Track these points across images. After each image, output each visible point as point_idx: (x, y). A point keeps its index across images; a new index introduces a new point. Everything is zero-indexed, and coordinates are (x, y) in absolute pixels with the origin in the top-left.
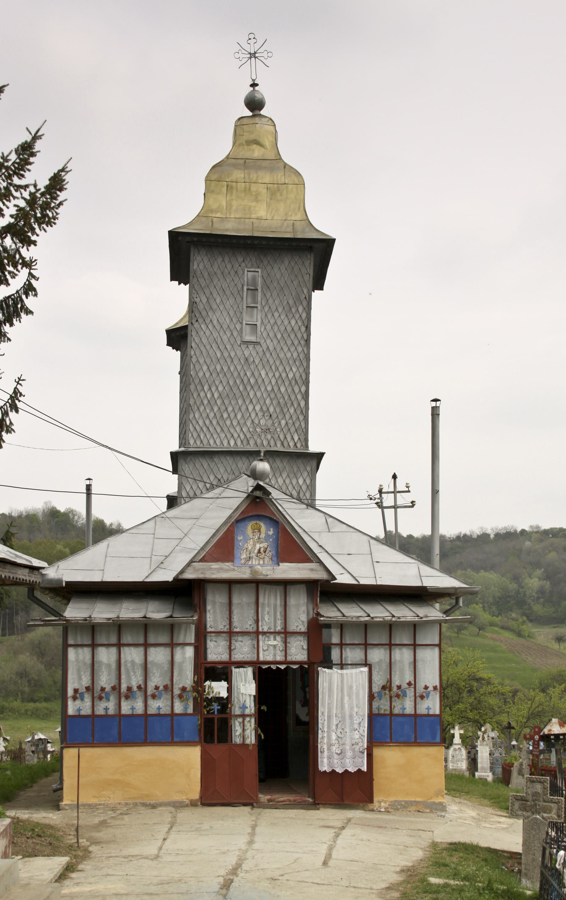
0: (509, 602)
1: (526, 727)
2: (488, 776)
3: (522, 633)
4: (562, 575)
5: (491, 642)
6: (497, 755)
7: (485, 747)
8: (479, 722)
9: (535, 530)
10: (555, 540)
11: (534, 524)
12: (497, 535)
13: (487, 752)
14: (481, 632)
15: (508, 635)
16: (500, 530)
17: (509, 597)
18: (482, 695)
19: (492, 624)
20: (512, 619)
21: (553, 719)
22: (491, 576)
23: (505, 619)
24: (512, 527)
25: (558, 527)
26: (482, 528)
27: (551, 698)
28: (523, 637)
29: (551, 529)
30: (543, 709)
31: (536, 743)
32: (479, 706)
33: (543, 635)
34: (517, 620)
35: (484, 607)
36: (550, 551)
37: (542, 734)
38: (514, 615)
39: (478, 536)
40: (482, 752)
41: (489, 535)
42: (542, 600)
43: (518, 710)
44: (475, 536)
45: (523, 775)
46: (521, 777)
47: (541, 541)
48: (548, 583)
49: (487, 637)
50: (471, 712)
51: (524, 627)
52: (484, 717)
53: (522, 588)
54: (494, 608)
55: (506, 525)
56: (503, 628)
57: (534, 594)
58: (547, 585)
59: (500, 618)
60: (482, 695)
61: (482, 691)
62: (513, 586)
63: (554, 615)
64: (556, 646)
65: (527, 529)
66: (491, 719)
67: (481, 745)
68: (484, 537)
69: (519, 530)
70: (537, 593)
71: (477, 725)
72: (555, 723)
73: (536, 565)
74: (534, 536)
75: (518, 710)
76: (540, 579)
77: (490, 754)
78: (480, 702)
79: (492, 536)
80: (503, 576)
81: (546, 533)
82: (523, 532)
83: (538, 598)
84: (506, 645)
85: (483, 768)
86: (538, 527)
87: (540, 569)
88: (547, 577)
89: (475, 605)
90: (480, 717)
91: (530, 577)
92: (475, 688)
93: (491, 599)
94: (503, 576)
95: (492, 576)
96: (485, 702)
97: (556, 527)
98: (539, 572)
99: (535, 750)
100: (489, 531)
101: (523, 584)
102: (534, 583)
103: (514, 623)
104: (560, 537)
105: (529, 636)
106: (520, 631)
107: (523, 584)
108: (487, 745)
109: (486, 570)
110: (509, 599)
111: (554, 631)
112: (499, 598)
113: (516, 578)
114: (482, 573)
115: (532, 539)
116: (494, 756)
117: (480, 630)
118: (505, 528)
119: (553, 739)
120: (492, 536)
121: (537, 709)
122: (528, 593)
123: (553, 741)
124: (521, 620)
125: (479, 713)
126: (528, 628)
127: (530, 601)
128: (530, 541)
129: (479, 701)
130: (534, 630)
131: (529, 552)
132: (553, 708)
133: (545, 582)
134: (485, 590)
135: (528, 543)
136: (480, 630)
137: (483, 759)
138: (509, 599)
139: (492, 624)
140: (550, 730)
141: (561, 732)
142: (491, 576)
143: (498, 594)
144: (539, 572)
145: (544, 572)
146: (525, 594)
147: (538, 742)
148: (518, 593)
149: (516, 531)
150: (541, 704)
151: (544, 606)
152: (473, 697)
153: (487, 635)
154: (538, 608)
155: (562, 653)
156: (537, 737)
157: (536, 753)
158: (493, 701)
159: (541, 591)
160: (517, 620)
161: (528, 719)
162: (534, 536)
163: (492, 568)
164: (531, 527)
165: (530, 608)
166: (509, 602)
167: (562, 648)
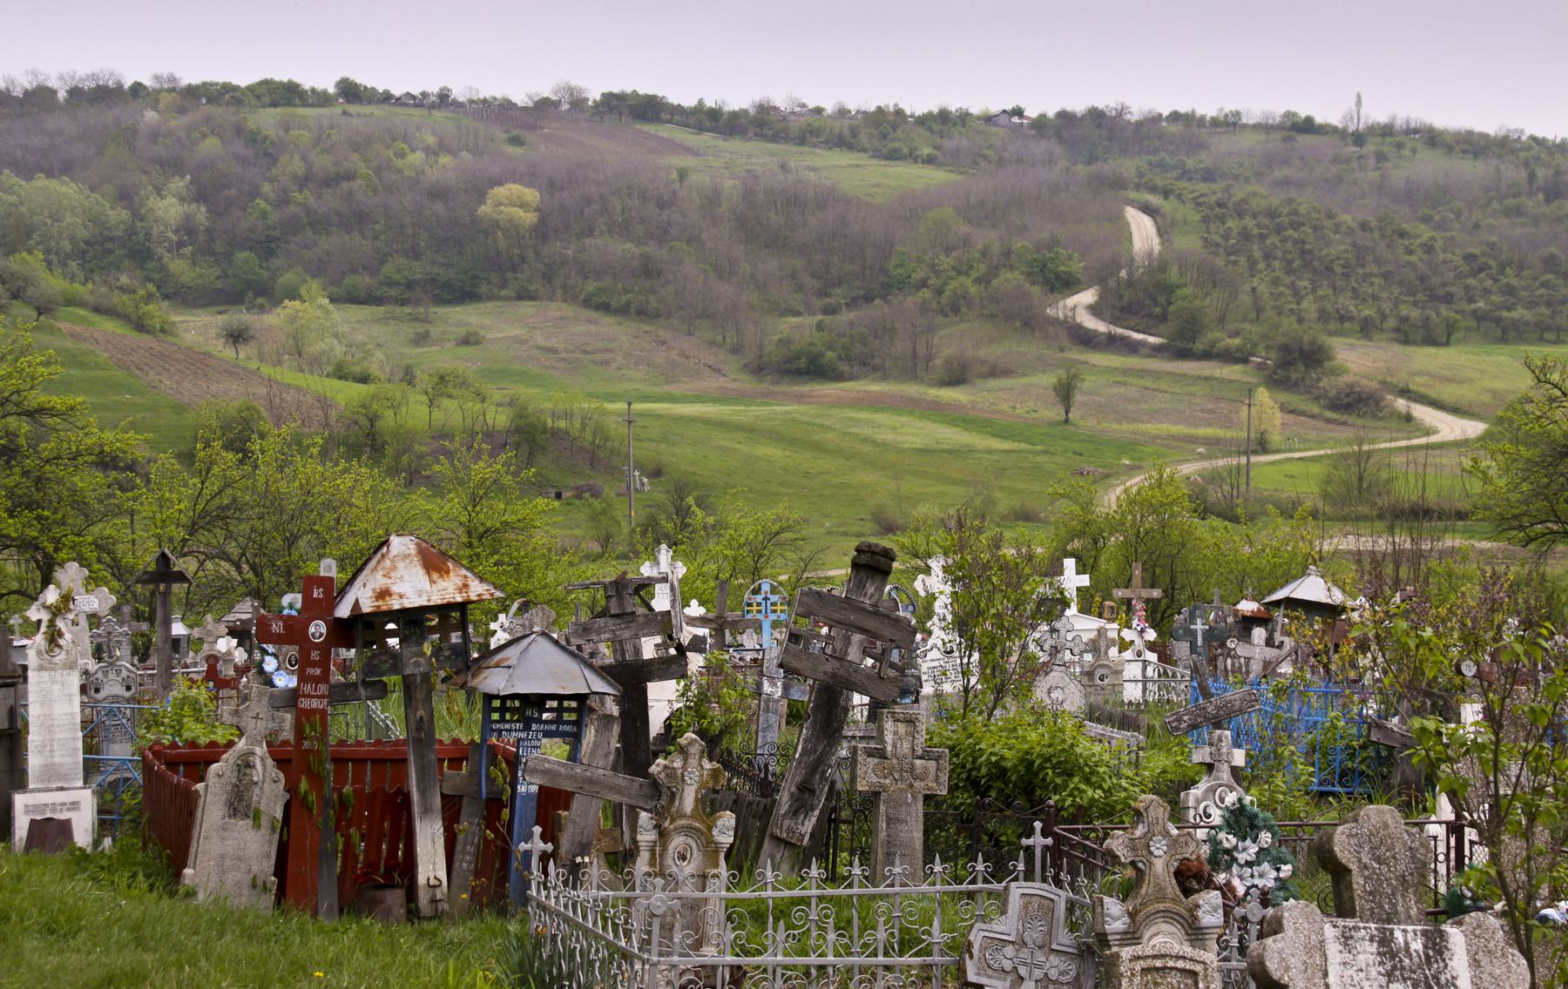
0: (110, 252)
1: (185, 555)
2: (75, 806)
3: (147, 322)
4: (233, 192)
5: (69, 344)
6: (112, 688)
7: (57, 675)
8: (37, 548)
9: (166, 86)
10: (217, 111)
11: (164, 70)
12: (75, 92)
13: (75, 749)
14: (42, 318)
15: (109, 326)
16: (81, 80)
17: (111, 239)
18: (48, 461)
19: (71, 302)
20: (121, 288)
21: (395, 541)
22: (64, 189)
23: (103, 289)
24: (111, 74)
25: (221, 81)
26: (35, 73)
27: (256, 467)
28: (148, 332)
29: (204, 84)
30: (234, 500)
31: (315, 655)
32: (37, 496)
33: (198, 328)
34: (134, 292)
35: (49, 263)
36: (205, 136)
37: (343, 611)
38: (124, 280)
39: (26, 93)
40: (47, 701)
41: (53, 92)
42: (188, 250)
43: (162, 503)
44: (18, 92)
45: (256, 816)
46: (243, 824)
47: (182, 111)
48: (203, 209)
49: (59, 330)
50: (11, 516)
51: (151, 307)
52: (57, 531)
53: (142, 220)
54: (74, 265)
55: (96, 70)
56: (97, 310)
57: (170, 234)
58: (201, 213)
59: (90, 286)
60: (48, 461)
61: (47, 448)
62: (118, 216)
63: (220, 285)
64: (229, 353)
65: (148, 82)
66: (79, 535)
67: (41, 668)
68: (41, 97)
69: (128, 84)
70: (176, 232)
71: (33, 557)
72: (406, 557)
73: (173, 166)
74: (165, 99)
75: (162, 503)
76: (182, 200)
77: (84, 689)
78: (39, 481)
79: (62, 95)
80: (92, 190)
81: (193, 92)
82: (137, 88)
83: (181, 244)
84: (106, 350)
85: (50, 772)
86: (172, 79)
87: (182, 176)
88: (201, 195)
89: (25, 254)
90: (41, 531)
91: (159, 195)
92: (22, 441)
93: (66, 246)
94: (92, 190)
95: (66, 190)
96: (60, 481)
97: (215, 80)
98: (179, 184)
99: (308, 688)
100: (53, 83)
101: (143, 211)
102: (169, 207)
103: (125, 298)
104: (228, 104)
105: (162, 330)
106: (140, 318)
107: (143, 211)
108: (71, 666)
109: (50, 174)
110: (109, 245)
111: (221, 319)
112: (87, 242)
113: (125, 196)
114: (41, 181)
115: (161, 106)
116: (100, 696)
117: (40, 314)
118: (94, 76)
119: (392, 634)
120: (62, 95)
121: (216, 501)
122: (155, 232)
123: (393, 642)
124: (141, 292)
125: (39, 518)
126: (158, 311)
127: (160, 251)
128: (155, 108)
129: (39, 480)
130: (176, 318)
131: (154, 136)
132: (265, 497)
133: (194, 206)
134: (49, 222)
135: (151, 115)
136: (40, 314)
137: (50, 730)
138: (109, 245)
139: (71, 302)
140: (383, 594)
141: (436, 600)
142: (64, 189)
143: (82, 233)
144: (179, 184)
145: (191, 183)
146: (148, 235)
147: (325, 648)
148: (131, 231)
149: (120, 86)
150: (228, 484)
151: (194, 263)
152: (17, 470)
153: (61, 325)
154: (178, 267)
155: (244, 369)
156: (318, 629)
157: (315, 704)
158: (88, 481)
159: (188, 228)
160: (134, 292)
161: (193, 529)
162: (165, 99)
163: (67, 169)
164: (157, 77)
165: (163, 268)
166: (110, 252)
167: (242, 355)
